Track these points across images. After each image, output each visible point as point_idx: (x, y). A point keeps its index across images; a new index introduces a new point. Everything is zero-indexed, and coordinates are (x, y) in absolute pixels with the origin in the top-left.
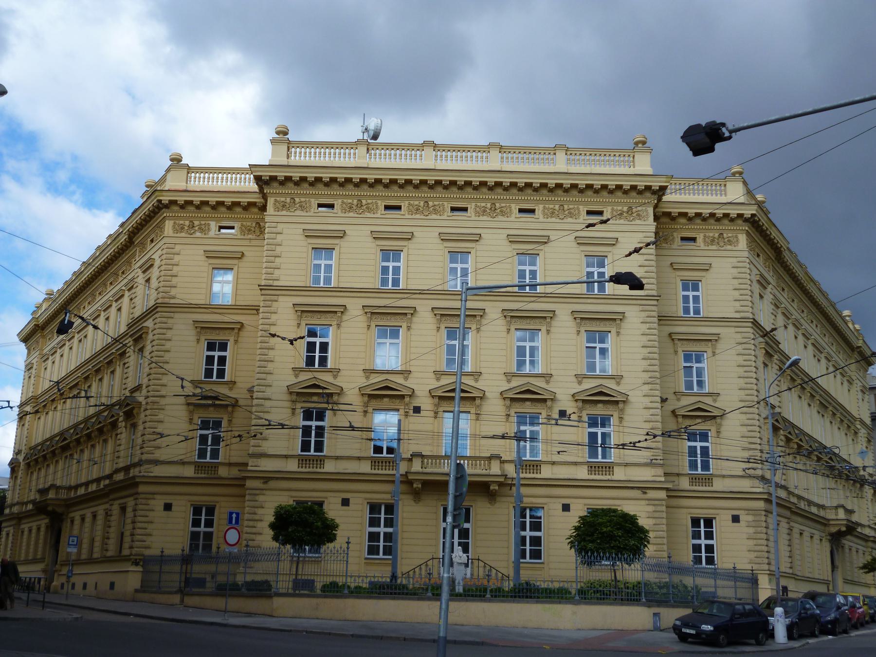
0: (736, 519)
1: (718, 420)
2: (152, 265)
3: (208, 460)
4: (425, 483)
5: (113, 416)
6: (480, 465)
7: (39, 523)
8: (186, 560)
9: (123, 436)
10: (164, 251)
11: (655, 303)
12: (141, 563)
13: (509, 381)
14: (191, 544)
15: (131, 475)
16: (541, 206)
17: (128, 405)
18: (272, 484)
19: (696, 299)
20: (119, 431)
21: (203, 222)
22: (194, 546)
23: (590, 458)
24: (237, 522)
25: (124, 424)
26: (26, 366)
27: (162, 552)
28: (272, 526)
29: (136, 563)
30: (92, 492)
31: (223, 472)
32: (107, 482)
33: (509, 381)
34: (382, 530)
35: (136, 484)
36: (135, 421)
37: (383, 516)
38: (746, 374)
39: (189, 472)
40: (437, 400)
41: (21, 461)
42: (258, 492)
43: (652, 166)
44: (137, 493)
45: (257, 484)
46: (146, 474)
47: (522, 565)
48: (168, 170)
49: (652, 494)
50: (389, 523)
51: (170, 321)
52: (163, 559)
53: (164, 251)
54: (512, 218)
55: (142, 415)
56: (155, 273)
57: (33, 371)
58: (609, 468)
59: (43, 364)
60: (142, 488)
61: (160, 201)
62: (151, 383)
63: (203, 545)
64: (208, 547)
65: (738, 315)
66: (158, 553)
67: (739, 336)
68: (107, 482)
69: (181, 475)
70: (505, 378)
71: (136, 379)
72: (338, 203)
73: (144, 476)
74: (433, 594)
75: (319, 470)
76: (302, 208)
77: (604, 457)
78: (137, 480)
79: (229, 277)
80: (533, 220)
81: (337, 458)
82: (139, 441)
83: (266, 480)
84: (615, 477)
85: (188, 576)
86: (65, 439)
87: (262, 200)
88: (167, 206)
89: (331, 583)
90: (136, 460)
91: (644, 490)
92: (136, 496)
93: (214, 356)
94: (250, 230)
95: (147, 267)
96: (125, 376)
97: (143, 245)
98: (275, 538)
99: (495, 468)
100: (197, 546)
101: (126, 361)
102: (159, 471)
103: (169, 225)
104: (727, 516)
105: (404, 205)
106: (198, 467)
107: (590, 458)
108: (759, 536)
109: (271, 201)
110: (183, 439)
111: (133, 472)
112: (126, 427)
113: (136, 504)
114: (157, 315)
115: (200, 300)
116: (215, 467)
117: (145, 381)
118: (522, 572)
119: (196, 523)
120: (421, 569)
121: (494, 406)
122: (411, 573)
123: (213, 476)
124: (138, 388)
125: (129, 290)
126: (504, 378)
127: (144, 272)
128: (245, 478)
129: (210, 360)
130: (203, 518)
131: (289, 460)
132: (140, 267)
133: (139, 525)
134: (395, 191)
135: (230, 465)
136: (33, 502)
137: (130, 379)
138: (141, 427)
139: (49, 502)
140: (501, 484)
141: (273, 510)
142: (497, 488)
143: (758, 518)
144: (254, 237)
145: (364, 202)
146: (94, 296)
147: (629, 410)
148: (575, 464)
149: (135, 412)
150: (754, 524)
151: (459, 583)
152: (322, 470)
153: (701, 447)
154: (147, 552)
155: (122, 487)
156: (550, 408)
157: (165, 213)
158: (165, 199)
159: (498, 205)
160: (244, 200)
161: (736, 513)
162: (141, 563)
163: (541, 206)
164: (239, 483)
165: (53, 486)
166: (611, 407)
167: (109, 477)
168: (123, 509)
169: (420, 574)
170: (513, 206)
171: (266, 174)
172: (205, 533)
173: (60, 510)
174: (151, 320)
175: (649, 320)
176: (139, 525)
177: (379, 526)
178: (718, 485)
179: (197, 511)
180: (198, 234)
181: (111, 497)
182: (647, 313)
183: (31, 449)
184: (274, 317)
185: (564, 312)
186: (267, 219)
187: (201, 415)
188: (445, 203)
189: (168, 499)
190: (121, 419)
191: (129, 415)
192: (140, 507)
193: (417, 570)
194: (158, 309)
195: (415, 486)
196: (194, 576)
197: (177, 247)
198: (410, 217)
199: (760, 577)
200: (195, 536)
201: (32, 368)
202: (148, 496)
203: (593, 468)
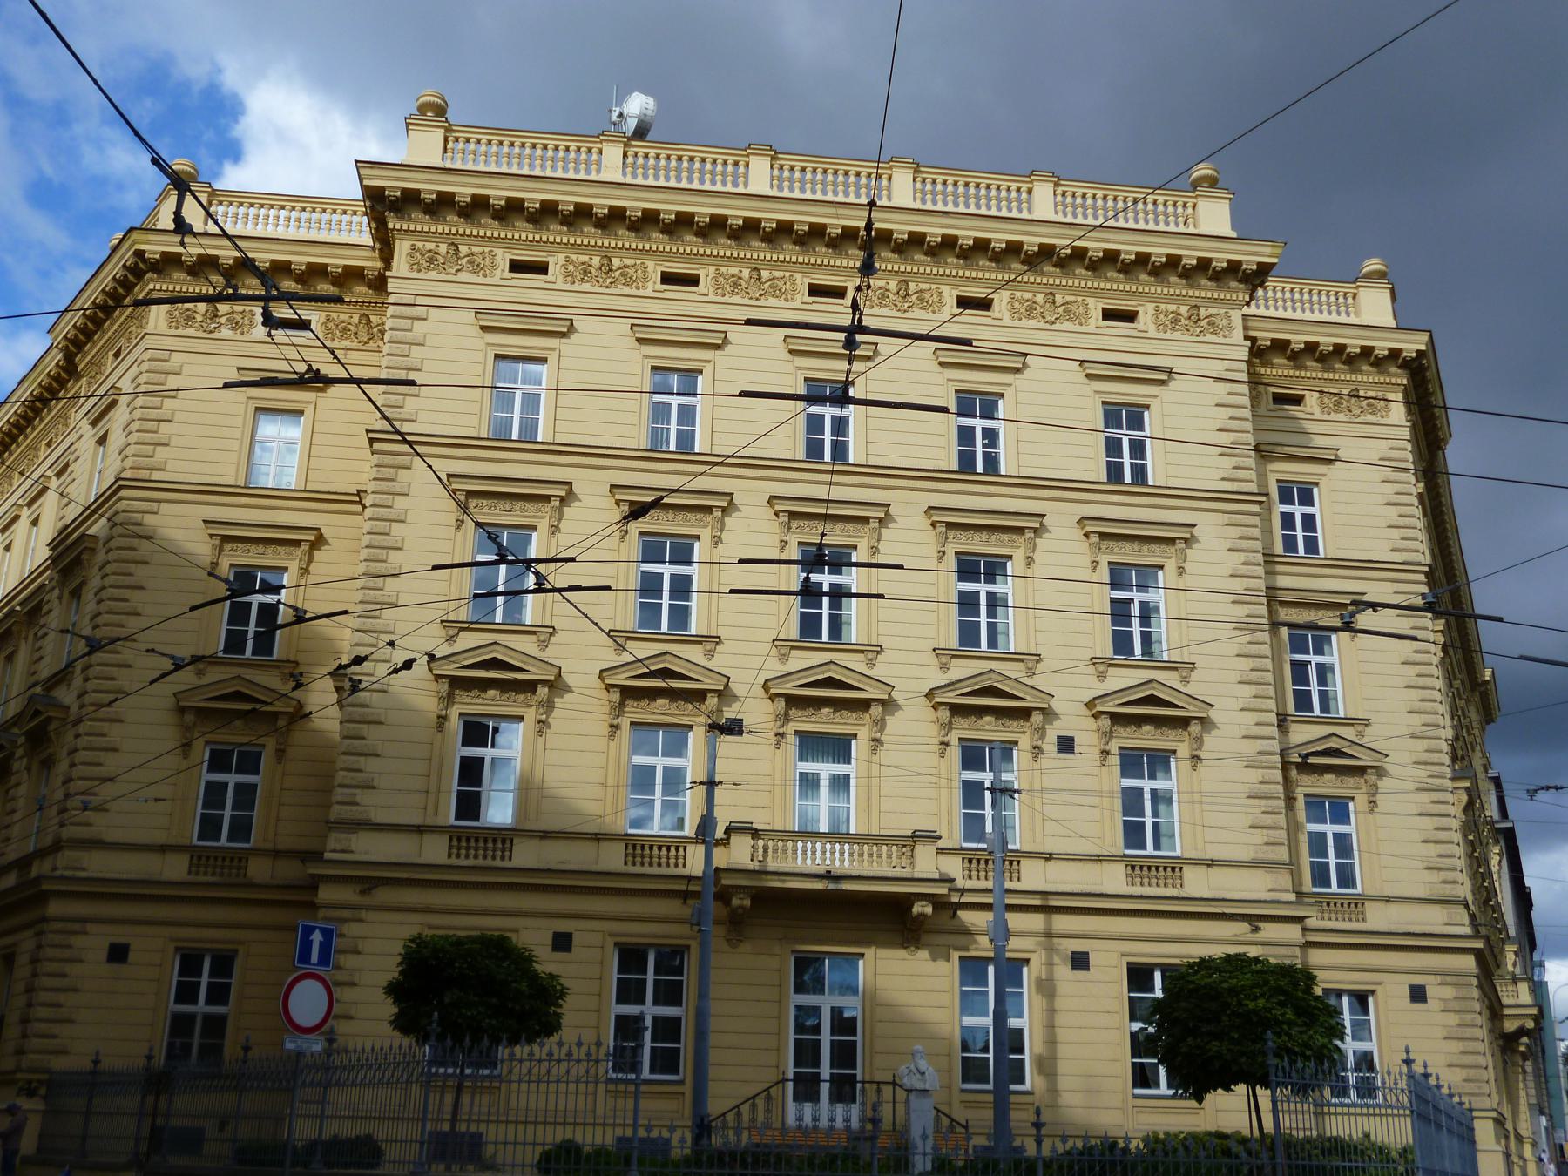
0: (1418, 994)
1: (1371, 777)
3: (224, 841)
6: (890, 856)
8: (156, 1082)
9: (22, 789)
10: (145, 367)
11: (1256, 508)
12: (43, 1091)
13: (944, 668)
14: (171, 1046)
18: (384, 895)
19: (1309, 521)
20: (14, 779)
22: (177, 1052)
23: (1127, 846)
24: (325, 958)
27: (96, 1062)
28: (394, 990)
29: (31, 1093)
31: (258, 870)
33: (944, 668)
34: (650, 1010)
35: (42, 898)
37: (650, 977)
38: (1421, 681)
39: (175, 868)
40: (781, 705)
42: (346, 914)
43: (1233, 228)
44: (44, 919)
45: (346, 894)
46: (68, 873)
47: (1013, 1098)
50: (670, 993)
52: (95, 1081)
53: (145, 367)
54: (1091, 328)
56: (120, 415)
58: (1173, 868)
60: (55, 908)
61: (140, 254)
63: (201, 1046)
64: (212, 1050)
65: (1398, 557)
66: (86, 1064)
69: (156, 878)
70: (935, 661)
72: (556, 262)
73: (62, 878)
75: (498, 863)
76: (476, 268)
77: (1157, 846)
78: (44, 887)
79: (293, 432)
80: (989, 321)
82: (59, 795)
83: (369, 885)
85: (160, 1121)
87: (379, 264)
89: (559, 1147)
90: (48, 840)
94: (345, 330)
96: (38, 655)
97: (97, 364)
98: (403, 1023)
99: (926, 862)
100: (187, 1048)
101: (42, 621)
102: (98, 865)
105: (706, 274)
106: (198, 857)
107: (1127, 846)
108: (1469, 1032)
109: (402, 249)
110: (167, 665)
112: (28, 769)
113: (39, 947)
115: (227, 474)
116: (241, 858)
119: (186, 993)
120: (754, 1106)
121: (914, 726)
122: (730, 1117)
125: (59, 475)
126: (933, 660)
127: (94, 423)
129: (215, 793)
130: (205, 980)
131: (427, 838)
133: (43, 996)
134: (690, 244)
135: (276, 854)
137: (47, 660)
138: (62, 767)
140: (939, 903)
141: (399, 948)
142: (929, 910)
143: (1464, 993)
145: (616, 262)
147: (1212, 743)
148: (1099, 858)
150: (1456, 1005)
152: (507, 864)
153: (1335, 835)
154: (59, 1064)
156: (1041, 732)
159: (912, 287)
160: (336, 261)
161: (1418, 980)
162: (43, 1091)
164: (302, 895)
169: (753, 1120)
170: (946, 289)
171: (394, 184)
172: (208, 1018)
175: (1244, 544)
176: (43, 996)
177: (642, 1001)
178: (1378, 918)
179: (190, 963)
180: (226, 333)
182: (1239, 531)
184: (400, 503)
185: (1062, 517)
188: (798, 276)
189: (120, 935)
190: (19, 752)
191: (39, 738)
192: (50, 952)
193: (745, 1109)
194: (124, 493)
195: (735, 902)
196: (174, 1122)
197: (176, 357)
199: (1477, 1124)
200: (181, 1025)
203: (1137, 868)
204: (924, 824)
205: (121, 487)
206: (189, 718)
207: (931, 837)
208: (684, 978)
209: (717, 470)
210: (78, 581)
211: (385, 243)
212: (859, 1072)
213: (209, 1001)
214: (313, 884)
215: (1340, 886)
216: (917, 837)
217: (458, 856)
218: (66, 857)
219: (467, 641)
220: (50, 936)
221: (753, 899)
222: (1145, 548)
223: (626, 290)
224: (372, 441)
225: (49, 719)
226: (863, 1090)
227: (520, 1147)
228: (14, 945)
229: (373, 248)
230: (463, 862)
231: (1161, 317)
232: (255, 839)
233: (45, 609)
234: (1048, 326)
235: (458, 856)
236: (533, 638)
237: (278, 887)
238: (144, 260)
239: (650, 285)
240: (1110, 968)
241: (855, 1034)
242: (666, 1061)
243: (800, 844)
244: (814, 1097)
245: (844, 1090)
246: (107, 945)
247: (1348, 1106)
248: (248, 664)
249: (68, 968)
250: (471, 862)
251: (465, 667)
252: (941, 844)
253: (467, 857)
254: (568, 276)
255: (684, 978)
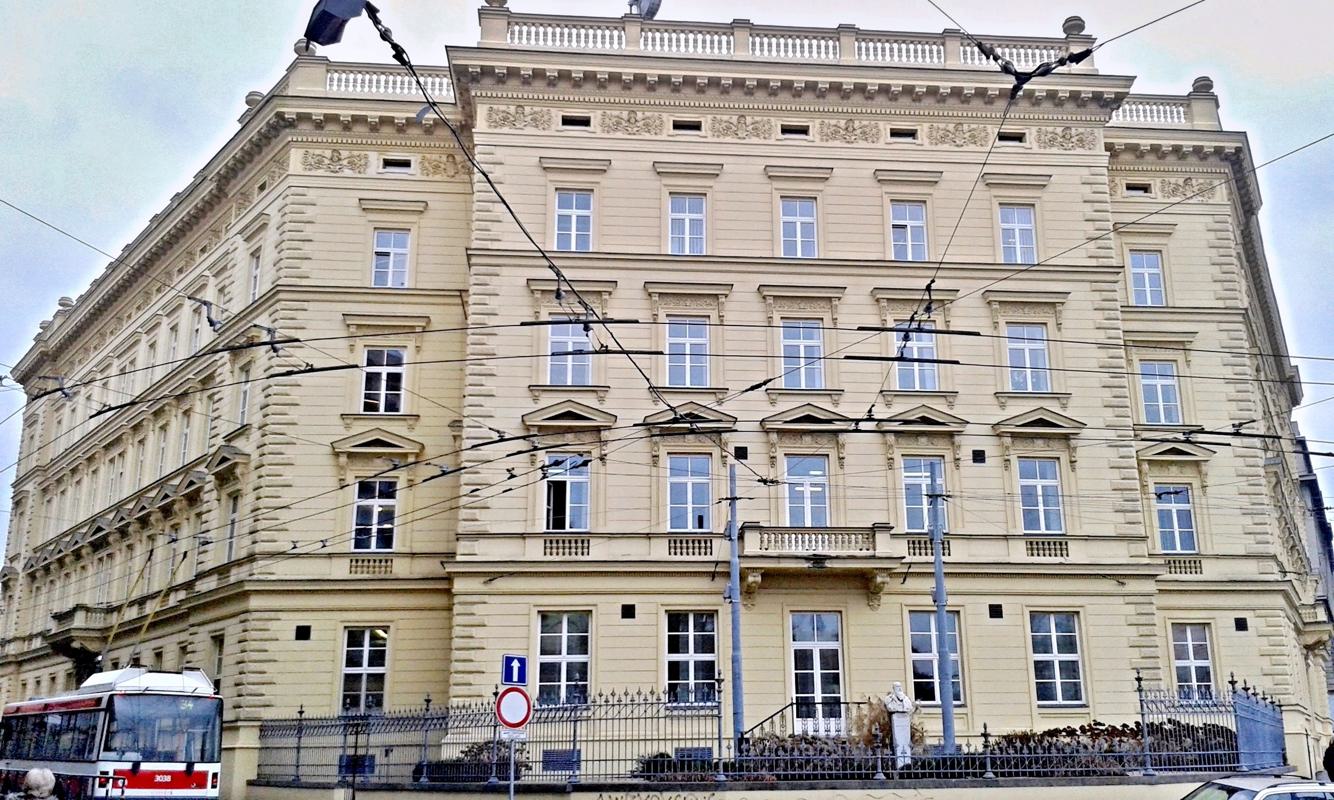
0: (1241, 625)
2: (264, 226)
4: (767, 575)
5: (192, 483)
7: (37, 673)
15: (232, 579)
16: (926, 126)
17: (224, 460)
18: (501, 584)
21: (356, 153)
25: (214, 494)
26: (26, 420)
30: (35, 651)
31: (401, 567)
32: (182, 595)
36: (238, 487)
37: (691, 633)
41: (20, 570)
45: (475, 585)
48: (291, 68)
49: (1133, 586)
51: (299, 315)
52: (300, 726)
54: (881, 144)
55: (254, 475)
56: (270, 237)
57: (38, 428)
58: (583, 540)
59: (56, 415)
60: (254, 602)
61: (280, 116)
62: (268, 420)
63: (1194, 647)
65: (1220, 304)
67: (1224, 335)
68: (182, 595)
71: (179, 458)
74: (996, 774)
75: (580, 557)
78: (247, 588)
81: (611, 536)
84: (1071, 559)
86: (100, 529)
88: (291, 124)
91: (1120, 579)
92: (243, 617)
93: (379, 374)
95: (252, 233)
97: (245, 196)
103: (295, 157)
104: (1224, 623)
109: (481, 111)
111: (235, 575)
114: (278, 306)
117: (256, 419)
118: (940, 727)
119: (353, 660)
123: (382, 576)
124: (243, 430)
127: (247, 240)
128: (449, 578)
129: (364, 514)
132: (240, 233)
134: (688, 96)
136: (43, 635)
139: (73, 634)
144: (445, 178)
146: (148, 295)
149: (238, 471)
151: (904, 752)
152: (586, 558)
155: (208, 606)
156: (956, 447)
157: (288, 136)
158: (290, 111)
163: (926, 126)
164: (443, 587)
165: (78, 608)
166: (1055, 444)
167: (188, 585)
168: (219, 640)
171: (475, 63)
173: (92, 647)
174: (267, 313)
180: (347, 172)
181: (192, 620)
183: (35, 550)
186: (477, 139)
187: (361, 474)
189: (303, 620)
190: (207, 487)
191: (225, 478)
194: (281, 296)
195: (751, 579)
198: (716, 140)
201: (35, 422)
202: (266, 615)
203: (1035, 544)
204: (881, 518)
205: (278, 292)
206: (343, 459)
207: (886, 528)
208: (715, 633)
209: (1020, 276)
210: (248, 359)
211: (467, 104)
212: (841, 695)
213: (371, 664)
214: (449, 578)
215: (1182, 549)
216: (874, 529)
217: (570, 554)
218: (259, 566)
219: (547, 400)
220: (253, 622)
221: (763, 575)
222: (1026, 310)
223: (647, 136)
224: (469, 256)
225: (236, 464)
226: (848, 709)
227: (616, 763)
228: (223, 629)
229: (455, 104)
230: (554, 558)
231: (607, 120)
232: (397, 546)
233: (218, 380)
234: (957, 149)
235: (551, 554)
236: (594, 394)
237: (432, 579)
238: (283, 119)
239: (882, 140)
240: (1017, 614)
241: (838, 669)
242: (708, 692)
243: (807, 536)
244: (811, 714)
245: (833, 708)
246: (295, 628)
247: (689, 708)
248: (381, 418)
249: (267, 645)
250: (560, 558)
251: (786, 422)
252: (893, 532)
253: (570, 554)
254: (826, 137)
255: (715, 633)
